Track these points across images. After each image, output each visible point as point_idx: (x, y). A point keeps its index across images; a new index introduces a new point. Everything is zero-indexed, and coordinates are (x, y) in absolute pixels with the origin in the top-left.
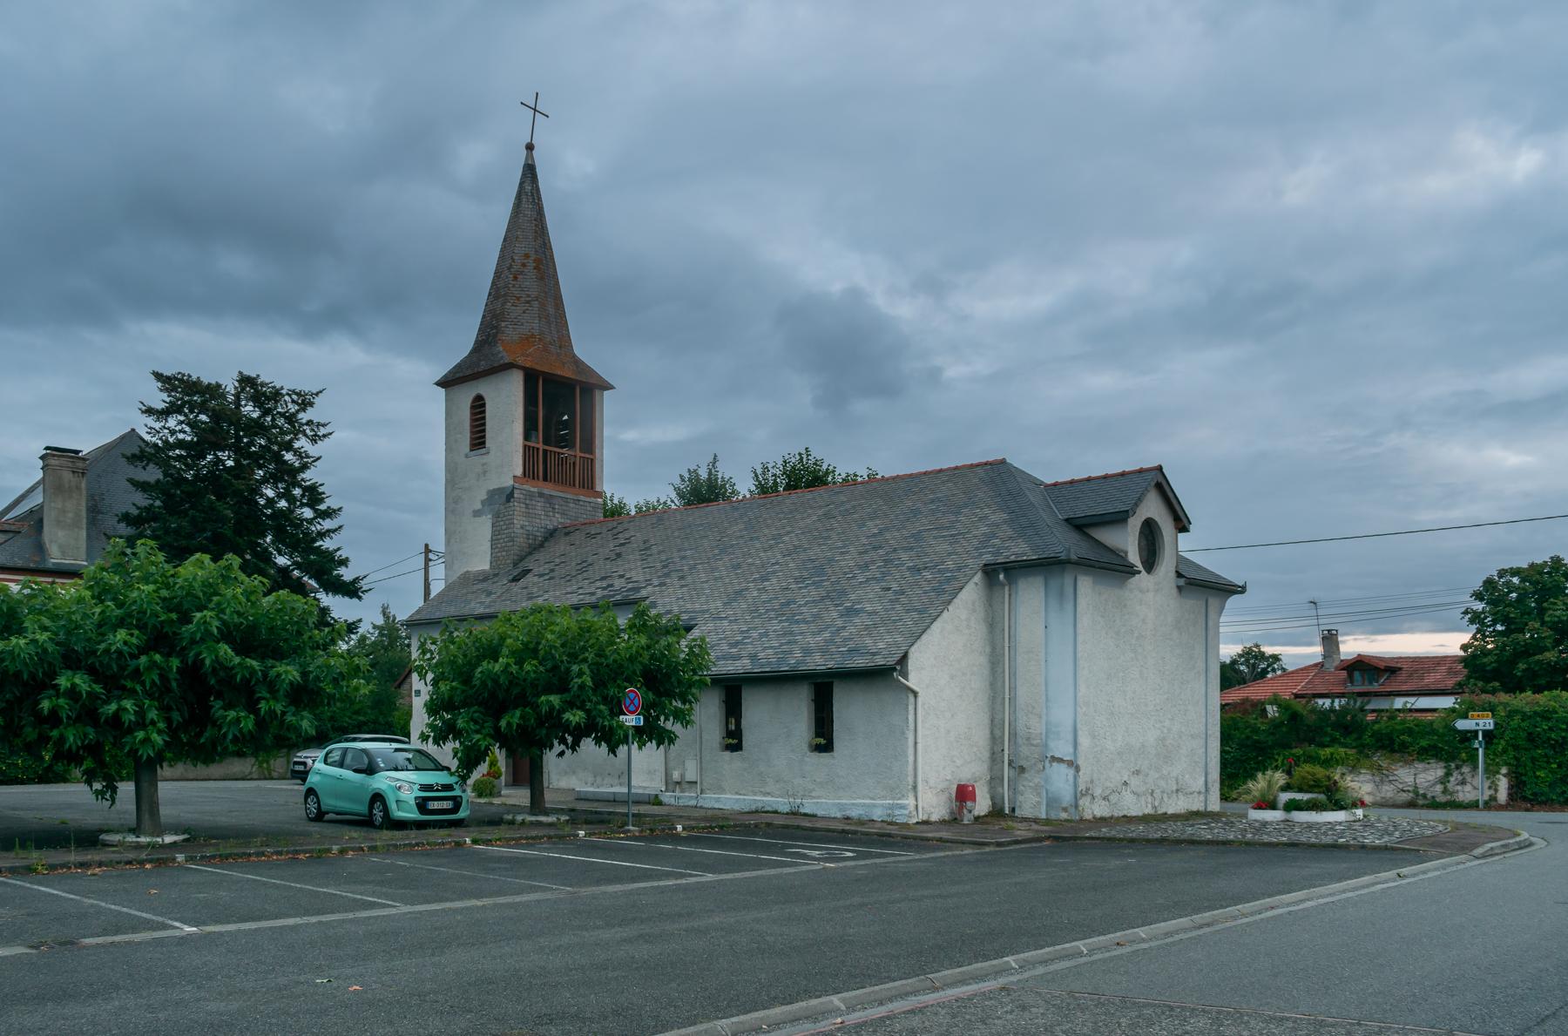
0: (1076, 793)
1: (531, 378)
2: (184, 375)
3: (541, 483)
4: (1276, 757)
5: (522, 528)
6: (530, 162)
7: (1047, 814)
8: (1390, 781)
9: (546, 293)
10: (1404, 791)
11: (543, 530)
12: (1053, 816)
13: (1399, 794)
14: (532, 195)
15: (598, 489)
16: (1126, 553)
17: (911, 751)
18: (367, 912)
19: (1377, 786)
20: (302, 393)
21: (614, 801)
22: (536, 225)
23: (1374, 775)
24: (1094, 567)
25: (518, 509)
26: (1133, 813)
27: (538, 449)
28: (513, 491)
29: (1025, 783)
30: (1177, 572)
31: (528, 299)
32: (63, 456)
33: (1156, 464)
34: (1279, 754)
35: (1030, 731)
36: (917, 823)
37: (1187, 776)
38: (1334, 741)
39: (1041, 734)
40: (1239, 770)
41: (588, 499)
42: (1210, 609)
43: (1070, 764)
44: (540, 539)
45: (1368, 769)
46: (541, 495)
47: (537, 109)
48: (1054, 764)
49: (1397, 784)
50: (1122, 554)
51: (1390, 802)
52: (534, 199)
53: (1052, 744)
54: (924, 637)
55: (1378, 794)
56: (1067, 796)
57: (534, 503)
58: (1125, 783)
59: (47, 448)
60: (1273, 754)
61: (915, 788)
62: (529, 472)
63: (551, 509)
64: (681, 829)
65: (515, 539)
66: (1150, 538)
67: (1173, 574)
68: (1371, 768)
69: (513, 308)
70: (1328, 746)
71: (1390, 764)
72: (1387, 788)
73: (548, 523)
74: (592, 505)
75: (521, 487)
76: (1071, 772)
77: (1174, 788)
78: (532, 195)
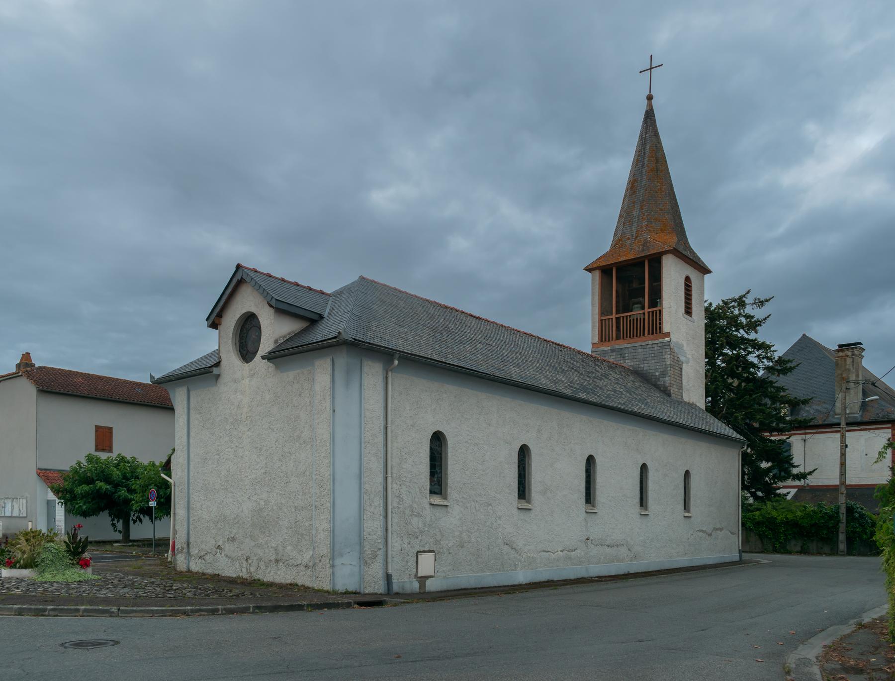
37: (289, 548)
41: (656, 342)
42: (336, 372)
74: (659, 345)
77: (273, 558)
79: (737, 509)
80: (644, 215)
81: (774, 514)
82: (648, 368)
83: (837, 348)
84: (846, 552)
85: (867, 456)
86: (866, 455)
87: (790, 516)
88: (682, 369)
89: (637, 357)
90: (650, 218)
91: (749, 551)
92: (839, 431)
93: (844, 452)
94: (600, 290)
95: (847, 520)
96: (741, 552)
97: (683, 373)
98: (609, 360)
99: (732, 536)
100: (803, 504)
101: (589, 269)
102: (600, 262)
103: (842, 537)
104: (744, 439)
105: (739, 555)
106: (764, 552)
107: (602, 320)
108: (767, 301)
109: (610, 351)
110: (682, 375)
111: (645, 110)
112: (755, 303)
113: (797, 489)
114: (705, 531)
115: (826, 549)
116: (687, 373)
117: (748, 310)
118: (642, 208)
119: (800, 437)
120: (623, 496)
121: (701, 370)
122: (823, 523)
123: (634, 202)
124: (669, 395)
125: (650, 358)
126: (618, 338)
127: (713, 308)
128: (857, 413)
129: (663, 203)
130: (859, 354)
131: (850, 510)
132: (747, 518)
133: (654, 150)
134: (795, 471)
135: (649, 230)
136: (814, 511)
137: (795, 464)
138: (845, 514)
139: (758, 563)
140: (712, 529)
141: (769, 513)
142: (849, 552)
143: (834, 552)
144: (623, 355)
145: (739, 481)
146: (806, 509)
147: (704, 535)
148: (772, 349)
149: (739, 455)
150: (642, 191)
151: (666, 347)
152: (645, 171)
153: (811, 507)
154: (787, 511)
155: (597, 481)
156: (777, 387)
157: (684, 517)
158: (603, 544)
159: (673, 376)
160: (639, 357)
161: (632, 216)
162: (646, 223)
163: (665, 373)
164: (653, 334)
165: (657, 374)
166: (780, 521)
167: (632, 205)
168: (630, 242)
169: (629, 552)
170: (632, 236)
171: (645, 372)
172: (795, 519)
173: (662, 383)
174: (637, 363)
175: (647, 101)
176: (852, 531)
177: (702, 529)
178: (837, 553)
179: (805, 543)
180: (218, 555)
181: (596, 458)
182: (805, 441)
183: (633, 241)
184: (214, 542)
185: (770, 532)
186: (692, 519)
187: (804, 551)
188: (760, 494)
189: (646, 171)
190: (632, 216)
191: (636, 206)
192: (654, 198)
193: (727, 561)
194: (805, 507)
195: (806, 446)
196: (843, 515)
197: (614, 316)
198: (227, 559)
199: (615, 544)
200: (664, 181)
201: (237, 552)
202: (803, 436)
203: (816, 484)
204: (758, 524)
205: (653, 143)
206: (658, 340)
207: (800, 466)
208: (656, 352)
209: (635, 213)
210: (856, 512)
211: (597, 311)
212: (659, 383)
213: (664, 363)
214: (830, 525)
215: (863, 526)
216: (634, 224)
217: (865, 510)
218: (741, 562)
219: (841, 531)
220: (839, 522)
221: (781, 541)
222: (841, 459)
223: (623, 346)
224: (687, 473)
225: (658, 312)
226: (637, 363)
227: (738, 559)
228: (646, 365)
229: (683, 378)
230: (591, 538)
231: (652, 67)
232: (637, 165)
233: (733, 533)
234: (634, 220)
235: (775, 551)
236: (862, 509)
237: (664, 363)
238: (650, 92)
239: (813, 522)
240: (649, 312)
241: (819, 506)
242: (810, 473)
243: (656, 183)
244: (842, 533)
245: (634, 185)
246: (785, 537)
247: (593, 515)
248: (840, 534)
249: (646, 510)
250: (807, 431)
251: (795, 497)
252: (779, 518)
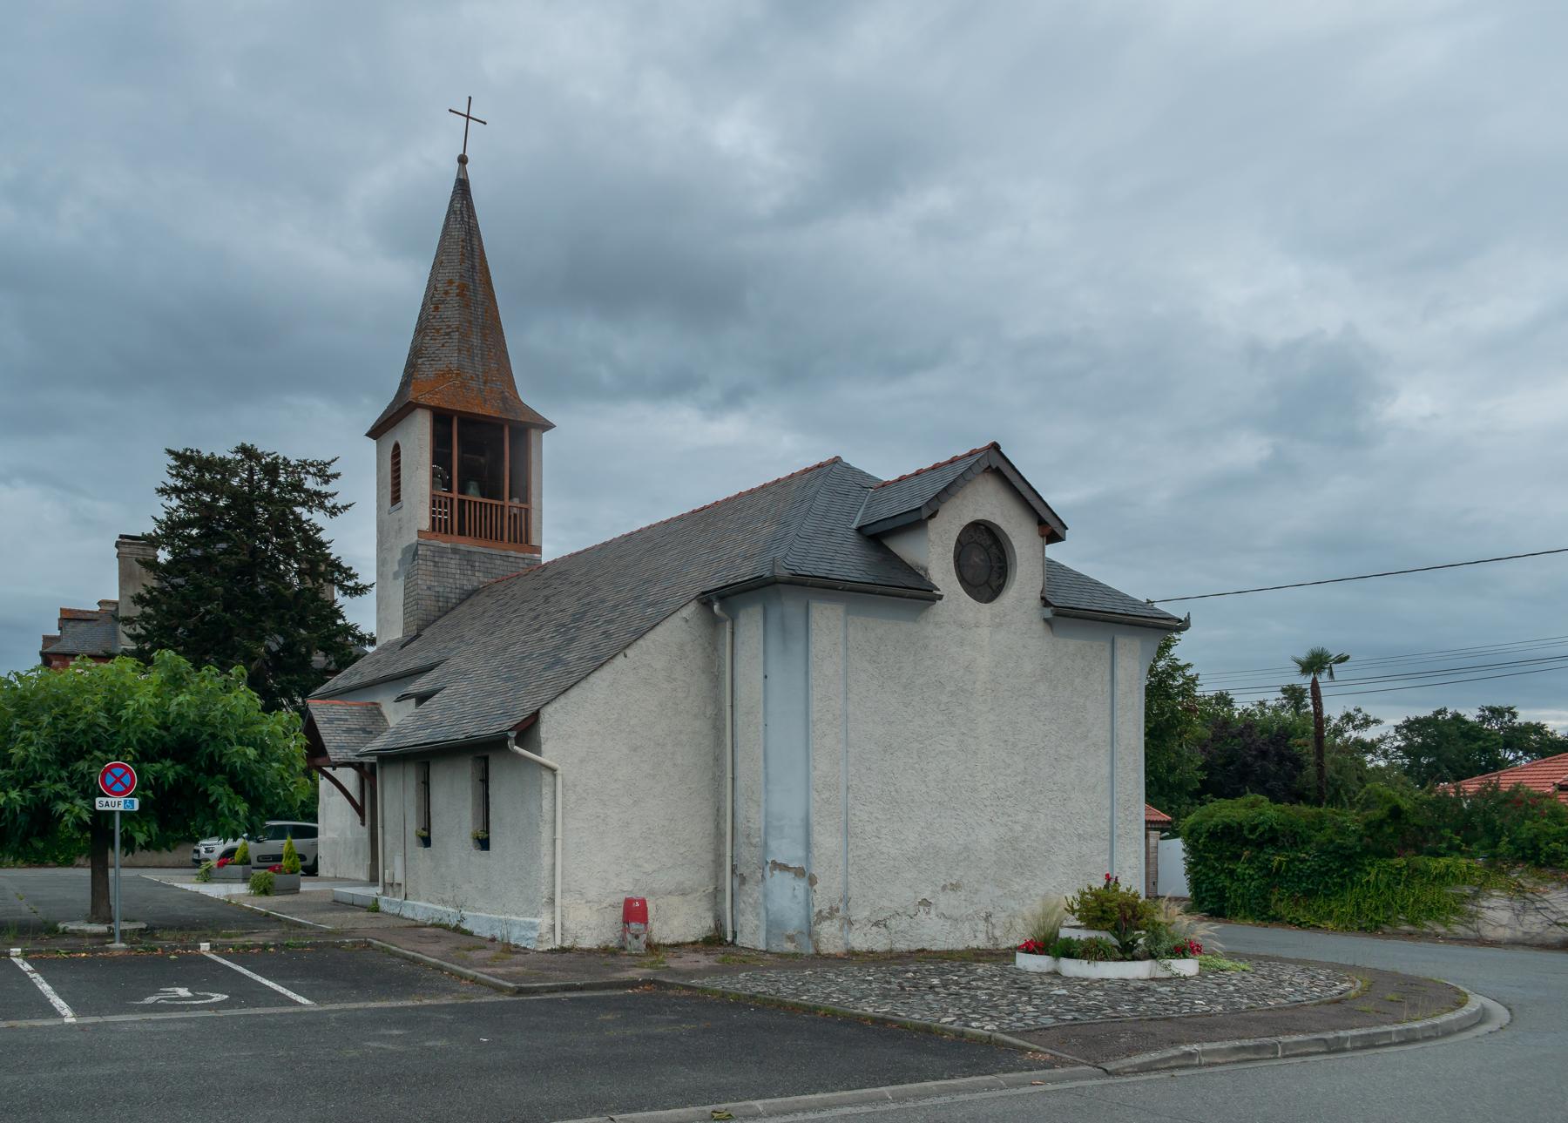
0: (808, 916)
1: (441, 419)
2: (192, 451)
3: (455, 537)
4: (1368, 869)
5: (429, 588)
6: (461, 177)
7: (767, 944)
8: (1537, 908)
9: (470, 322)
10: (1559, 925)
11: (457, 591)
12: (774, 948)
13: (1552, 929)
14: (462, 213)
15: (534, 542)
16: (926, 570)
17: (546, 849)
18: (121, 1016)
19: (1518, 915)
20: (315, 463)
21: (353, 905)
22: (463, 247)
23: (1511, 899)
24: (837, 589)
25: (424, 567)
26: (940, 945)
27: (452, 499)
28: (417, 547)
29: (745, 899)
30: (1043, 598)
31: (447, 331)
32: (134, 544)
33: (986, 444)
34: (1372, 865)
35: (750, 825)
36: (552, 951)
38: (1453, 849)
39: (759, 829)
40: (1319, 884)
41: (522, 555)
43: (800, 873)
44: (454, 601)
45: (1502, 889)
46: (455, 551)
47: (466, 118)
48: (776, 873)
49: (1548, 914)
50: (922, 573)
51: (1538, 940)
52: (463, 217)
53: (773, 844)
54: (574, 693)
55: (1518, 927)
56: (795, 922)
57: (445, 560)
58: (925, 903)
59: (121, 537)
60: (1364, 865)
61: (552, 901)
62: (437, 526)
63: (469, 567)
64: (208, 948)
65: (419, 602)
66: (994, 550)
67: (1034, 601)
68: (1507, 888)
69: (432, 342)
70: (1444, 855)
71: (1536, 883)
72: (1532, 918)
73: (465, 582)
74: (526, 561)
75: (427, 542)
76: (801, 885)
78: (462, 213)
109: (450, 551)
144: (471, 563)
180: (922, 915)
184: (913, 895)
198: (942, 922)
201: (966, 907)
206: (524, 553)
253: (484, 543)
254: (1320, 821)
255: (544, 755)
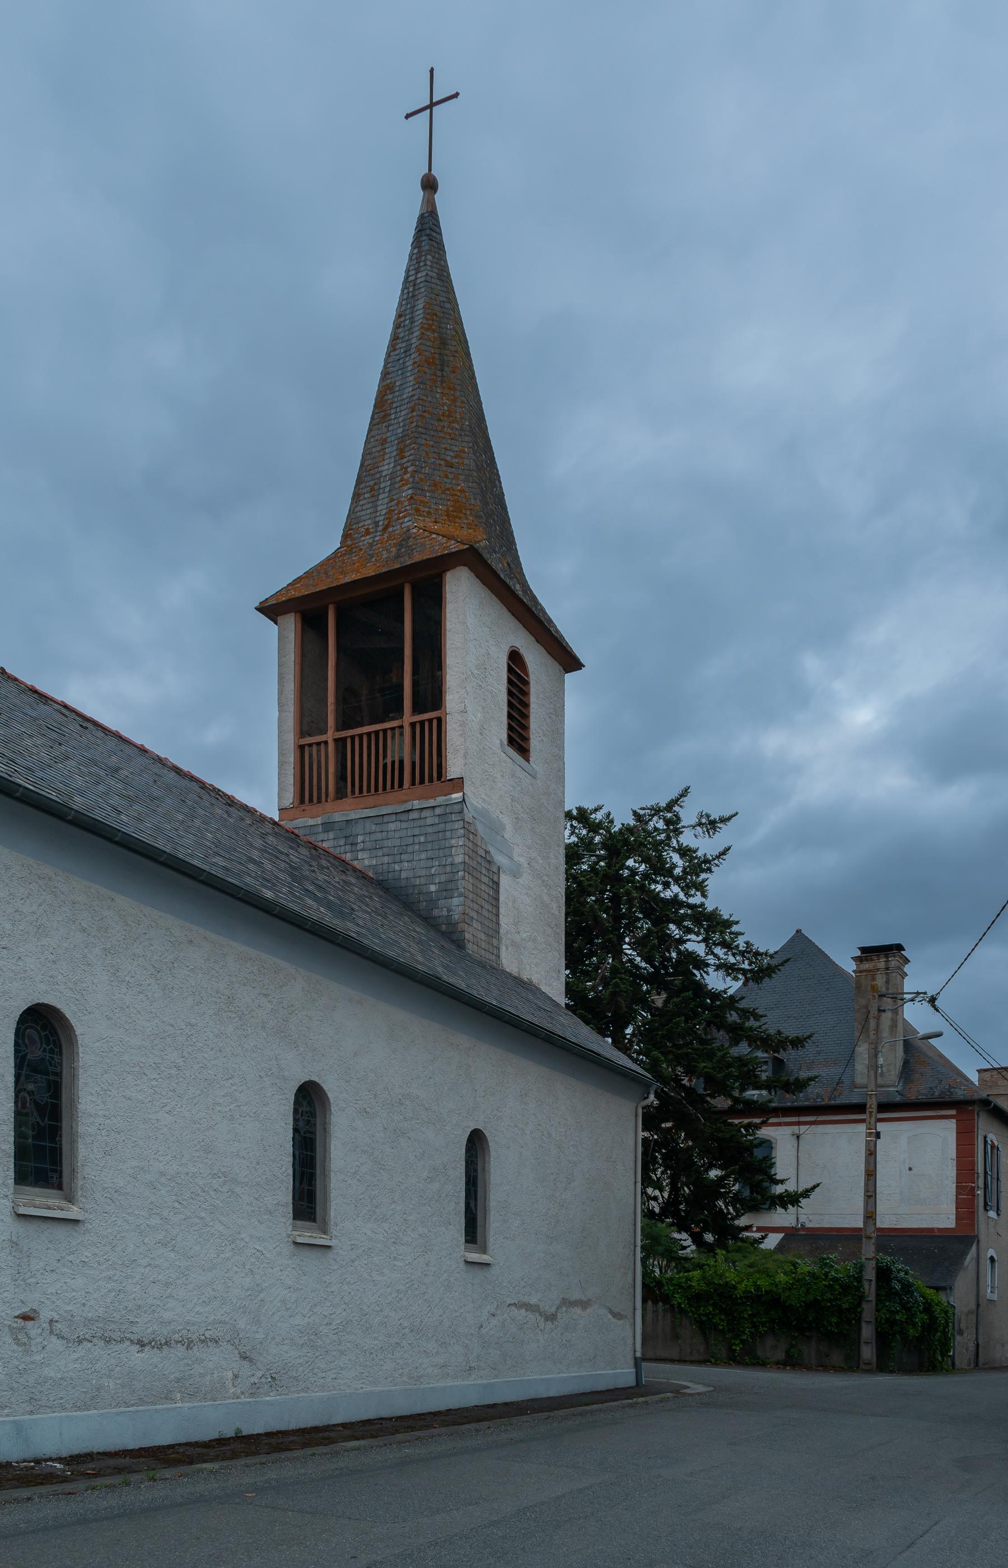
41: (431, 803)
47: (434, 108)
74: (438, 811)
79: (632, 1254)
80: (406, 473)
81: (731, 1276)
82: (410, 874)
83: (858, 953)
84: (874, 1366)
85: (912, 1172)
86: (910, 1169)
87: (763, 1283)
88: (497, 884)
89: (386, 843)
90: (421, 480)
91: (677, 1358)
92: (863, 1121)
93: (872, 1149)
94: (298, 668)
95: (878, 1295)
96: (637, 1363)
97: (502, 898)
98: (312, 839)
99: (615, 1320)
100: (790, 1258)
101: (271, 610)
102: (295, 590)
103: (867, 1332)
104: (649, 1076)
105: (634, 1370)
106: (711, 1362)
107: (302, 748)
108: (724, 820)
110: (497, 900)
111: (417, 214)
112: (700, 824)
113: (783, 1235)
114: (537, 1306)
115: (836, 1358)
116: (514, 902)
117: (687, 839)
118: (401, 453)
119: (787, 1131)
120: (214, 1176)
121: (554, 905)
122: (830, 1300)
123: (384, 441)
124: (460, 945)
125: (417, 847)
126: (341, 794)
127: (616, 829)
128: (893, 1086)
129: (456, 449)
130: (899, 968)
131: (884, 1274)
132: (674, 1285)
133: (436, 315)
134: (779, 1189)
135: (417, 510)
136: (812, 1275)
137: (778, 1177)
138: (873, 1283)
139: (678, 1391)
140: (557, 1302)
141: (721, 1276)
142: (882, 1366)
143: (852, 1365)
145: (635, 1183)
146: (796, 1268)
147: (532, 1317)
148: (735, 928)
149: (636, 1116)
150: (403, 413)
151: (454, 817)
152: (411, 362)
153: (806, 1266)
154: (758, 1272)
155: (81, 1107)
156: (743, 1010)
157: (467, 1262)
158: (116, 1336)
159: (471, 896)
160: (389, 843)
161: (378, 476)
162: (410, 492)
163: (450, 887)
164: (422, 782)
165: (433, 888)
166: (745, 1292)
167: (379, 448)
168: (371, 541)
169: (246, 1363)
170: (376, 524)
171: (403, 883)
172: (774, 1289)
173: (445, 913)
174: (386, 859)
175: (422, 193)
176: (887, 1320)
177: (525, 1299)
178: (858, 1367)
179: (794, 1343)
181: (73, 1022)
182: (798, 1137)
183: (377, 538)
185: (723, 1317)
186: (494, 1271)
187: (791, 1362)
188: (709, 1237)
189: (414, 363)
190: (378, 476)
191: (387, 451)
192: (432, 433)
193: (601, 1387)
194: (795, 1265)
195: (800, 1148)
196: (870, 1285)
197: (330, 736)
199: (176, 1336)
200: (458, 394)
202: (795, 1128)
203: (817, 1226)
204: (697, 1298)
205: (433, 296)
206: (433, 797)
207: (787, 1182)
208: (430, 830)
209: (386, 467)
210: (896, 1278)
211: (290, 722)
212: (436, 913)
213: (450, 860)
214: (845, 1306)
215: (908, 1309)
216: (381, 497)
217: (912, 1276)
218: (638, 1390)
219: (867, 1320)
220: (861, 1298)
221: (744, 1337)
222: (867, 1162)
223: (353, 815)
224: (476, 1142)
225: (435, 722)
226: (386, 859)
227: (631, 1381)
228: (406, 864)
229: (502, 911)
230: (46, 1314)
231: (434, 100)
232: (395, 350)
233: (617, 1315)
234: (382, 485)
235: (734, 1360)
236: (906, 1273)
237: (450, 860)
238: (430, 169)
239: (811, 1297)
240: (413, 725)
241: (823, 1263)
242: (806, 1193)
243: (438, 396)
244: (868, 1322)
245: (386, 397)
246: (753, 1330)
247: (60, 1232)
248: (864, 1325)
249: (325, 1233)
250: (803, 1119)
251: (780, 1247)
252: (742, 1287)
253: (371, 800)
254: (668, 822)
255: (333, 1230)
